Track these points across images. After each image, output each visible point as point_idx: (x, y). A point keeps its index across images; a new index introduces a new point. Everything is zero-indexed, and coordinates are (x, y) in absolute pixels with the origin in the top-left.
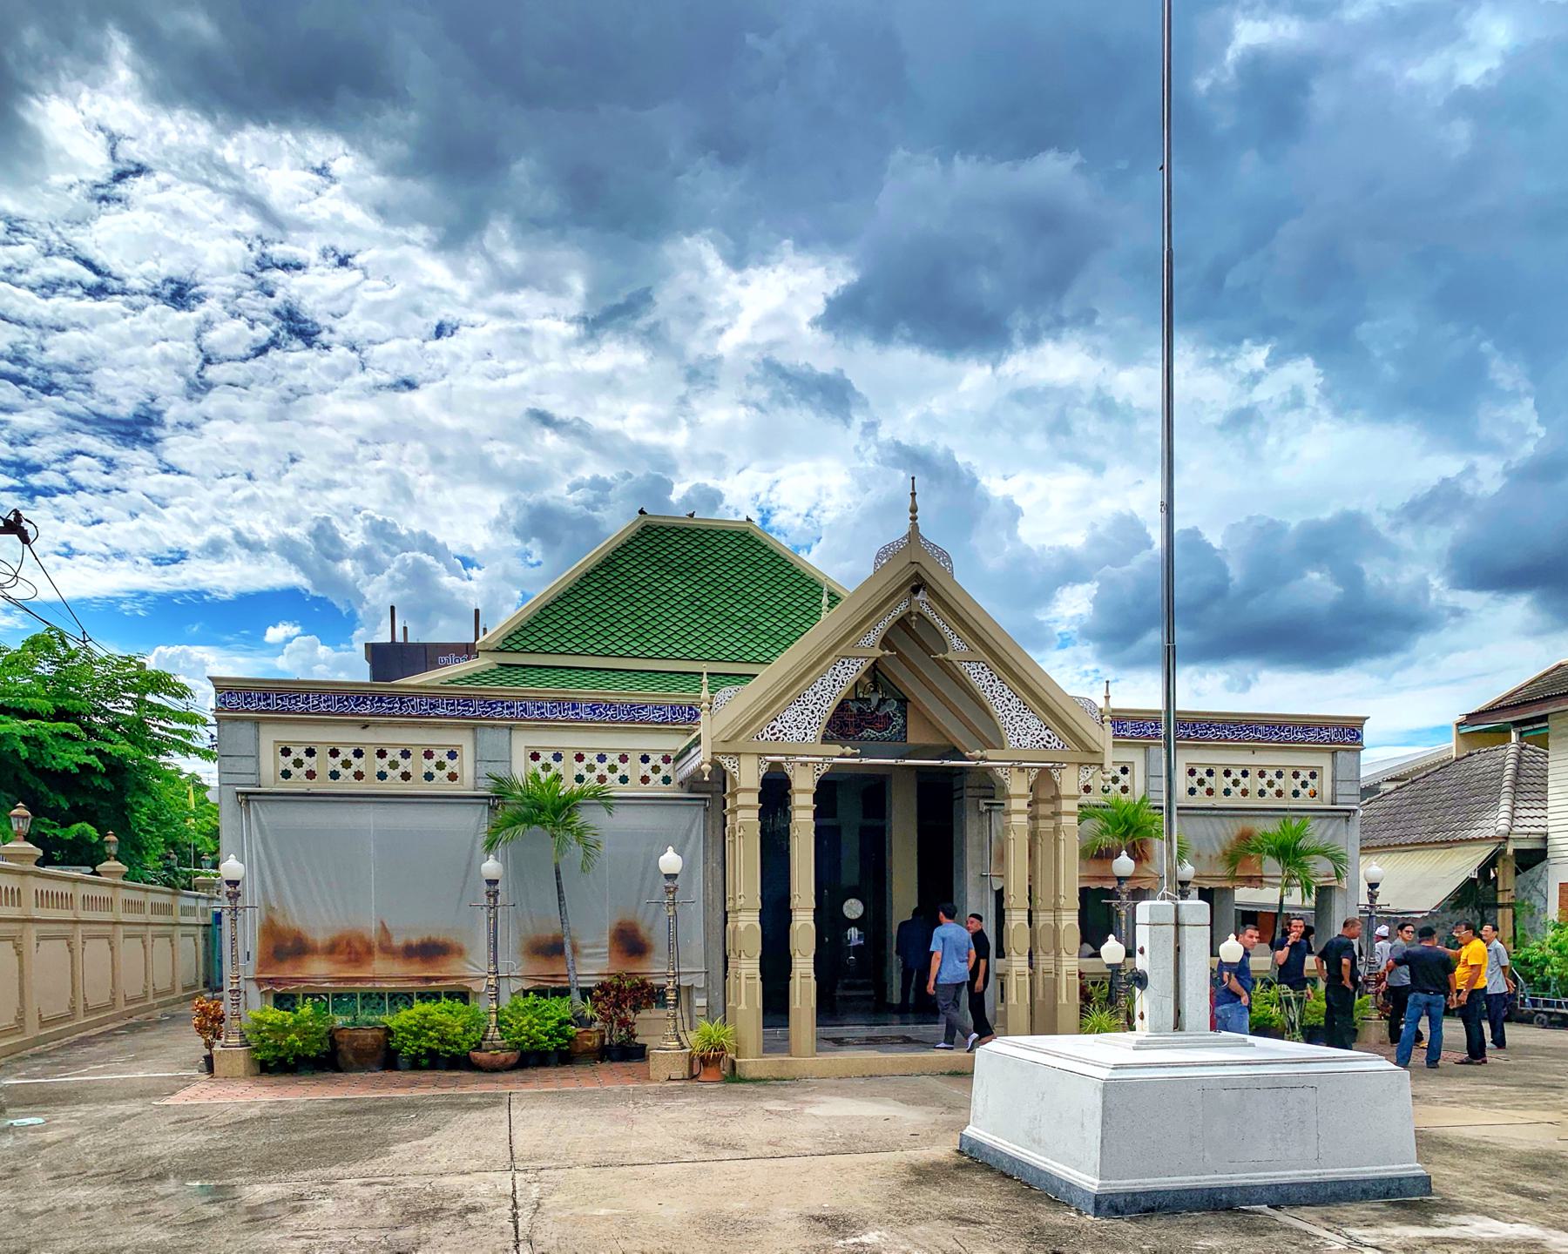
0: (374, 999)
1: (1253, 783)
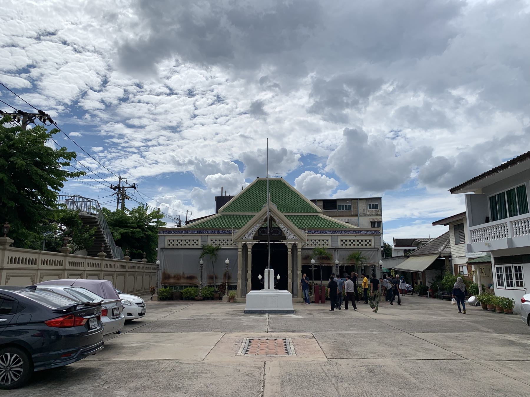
0: (182, 287)
1: (356, 243)
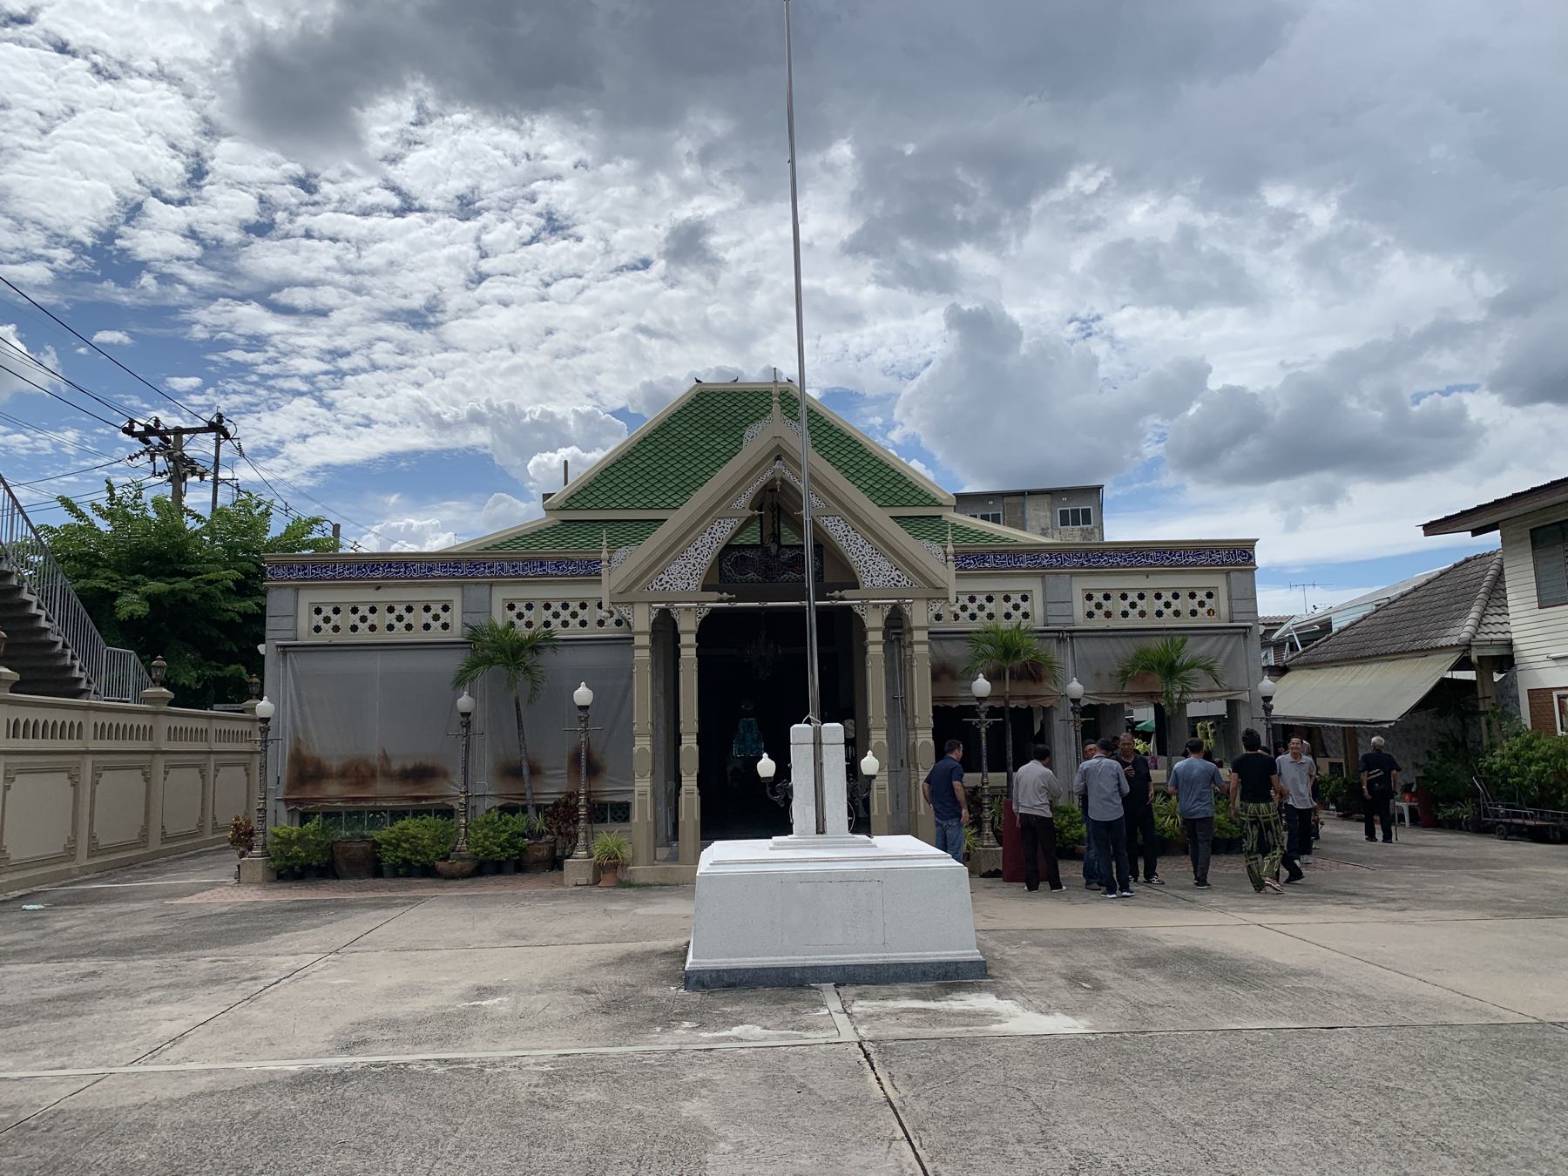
0: (377, 816)
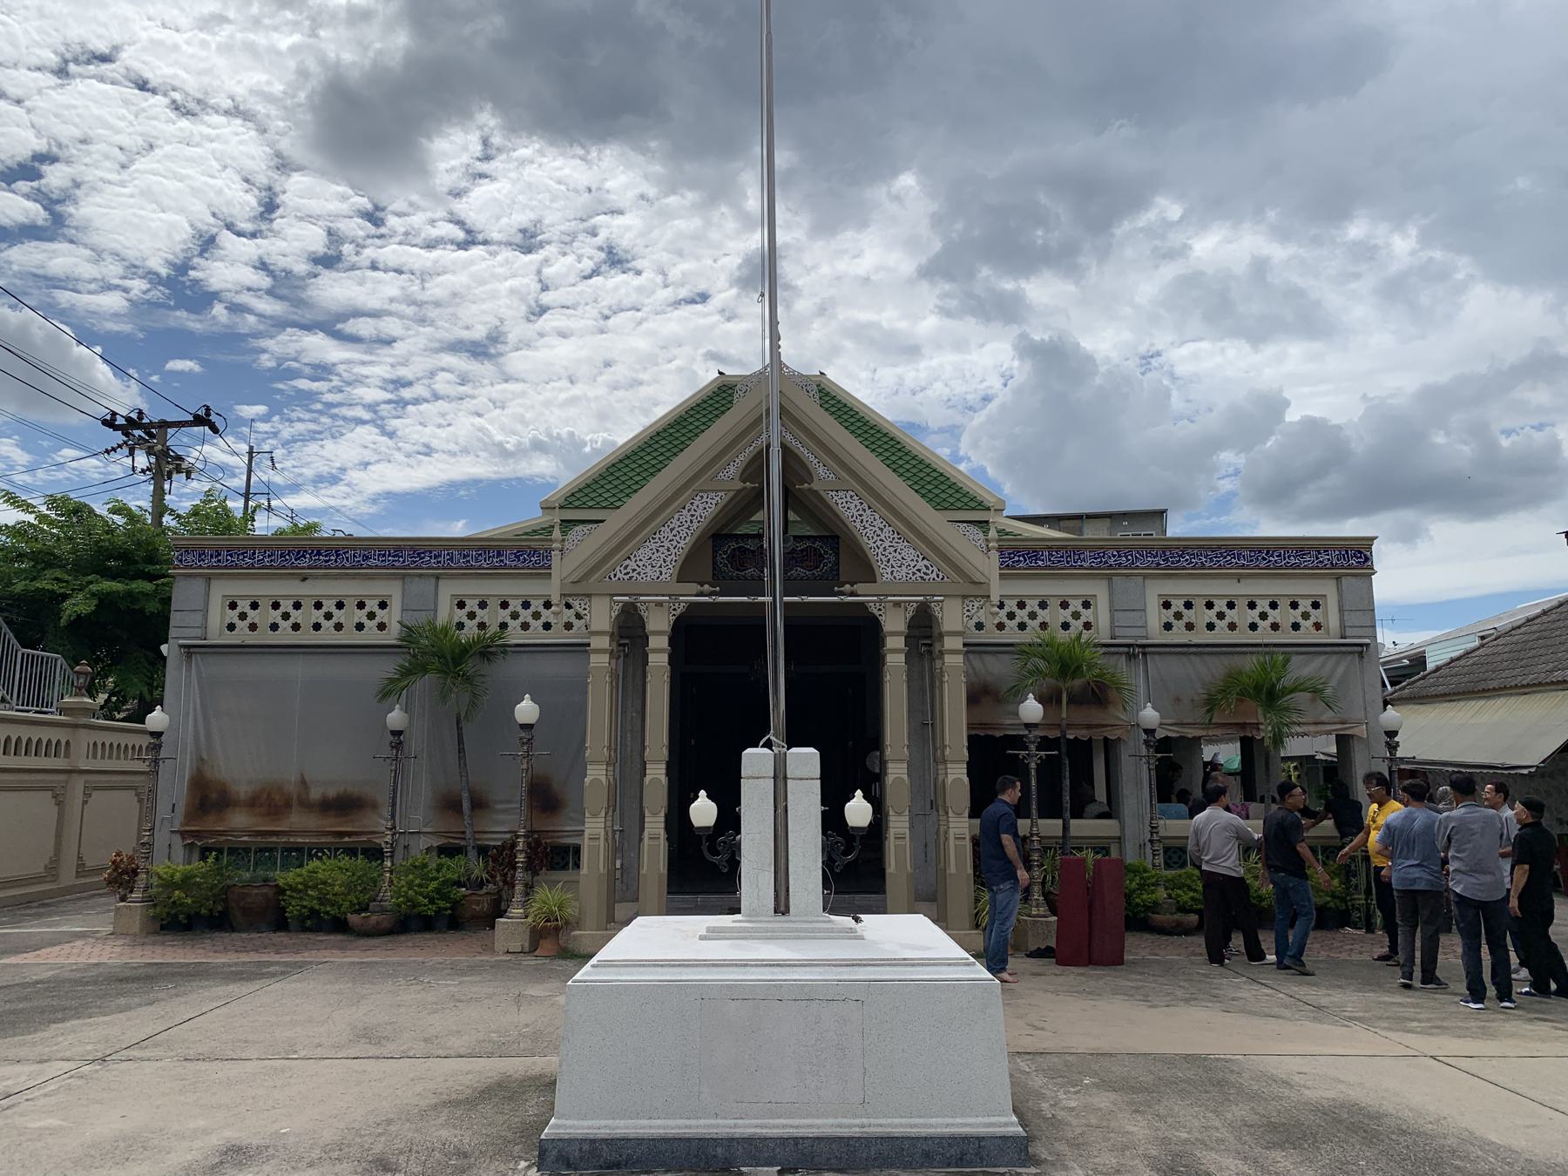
0: (298, 854)
